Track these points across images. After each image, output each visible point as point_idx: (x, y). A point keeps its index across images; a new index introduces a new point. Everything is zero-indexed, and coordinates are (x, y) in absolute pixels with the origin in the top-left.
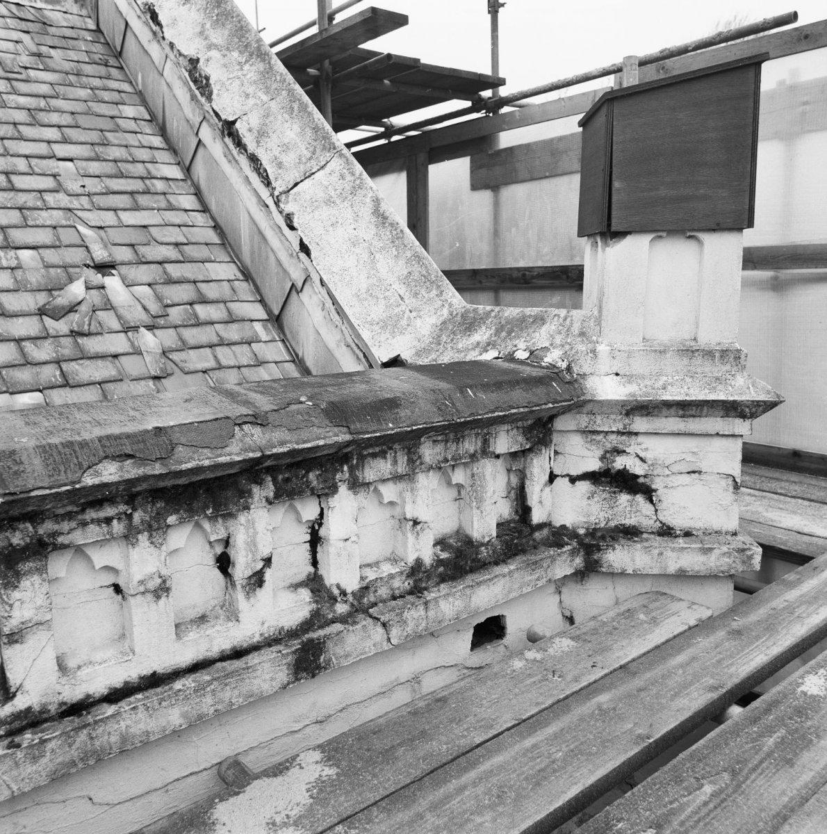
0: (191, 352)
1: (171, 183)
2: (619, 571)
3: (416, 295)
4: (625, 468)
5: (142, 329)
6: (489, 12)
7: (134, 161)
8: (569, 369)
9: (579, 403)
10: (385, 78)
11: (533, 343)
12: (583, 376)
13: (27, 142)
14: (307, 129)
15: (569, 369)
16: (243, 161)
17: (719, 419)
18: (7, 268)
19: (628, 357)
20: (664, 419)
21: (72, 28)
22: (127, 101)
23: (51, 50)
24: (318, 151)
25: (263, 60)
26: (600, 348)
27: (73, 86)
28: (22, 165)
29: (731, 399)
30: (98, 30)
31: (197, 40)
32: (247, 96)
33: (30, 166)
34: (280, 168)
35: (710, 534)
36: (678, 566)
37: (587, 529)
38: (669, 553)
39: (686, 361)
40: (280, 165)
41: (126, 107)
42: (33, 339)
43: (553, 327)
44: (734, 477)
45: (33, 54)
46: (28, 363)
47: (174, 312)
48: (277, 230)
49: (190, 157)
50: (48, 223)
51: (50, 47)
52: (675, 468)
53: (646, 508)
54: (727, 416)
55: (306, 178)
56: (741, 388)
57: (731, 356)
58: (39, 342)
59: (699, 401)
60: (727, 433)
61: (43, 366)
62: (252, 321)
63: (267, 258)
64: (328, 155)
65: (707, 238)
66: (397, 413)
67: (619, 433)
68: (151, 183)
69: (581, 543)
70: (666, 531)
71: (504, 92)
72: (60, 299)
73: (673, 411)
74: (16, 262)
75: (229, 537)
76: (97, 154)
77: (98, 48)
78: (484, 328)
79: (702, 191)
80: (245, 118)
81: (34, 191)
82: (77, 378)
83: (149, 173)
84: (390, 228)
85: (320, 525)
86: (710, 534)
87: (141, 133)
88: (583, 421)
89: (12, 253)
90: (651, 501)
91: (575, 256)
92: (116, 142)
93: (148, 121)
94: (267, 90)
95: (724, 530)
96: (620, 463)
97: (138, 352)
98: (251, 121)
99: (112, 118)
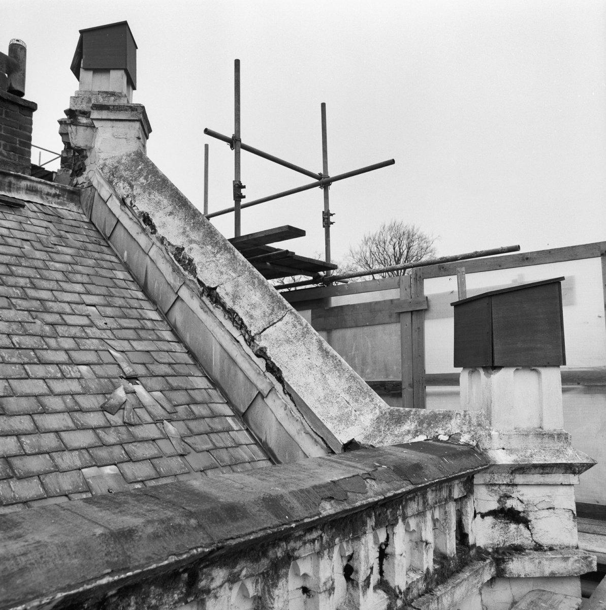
0: (197, 437)
1: (154, 322)
2: (517, 576)
3: (357, 401)
4: (512, 507)
5: (165, 421)
6: (324, 226)
7: (131, 308)
8: (477, 445)
9: (489, 466)
10: (268, 261)
11: (449, 431)
12: (485, 450)
13: (67, 293)
14: (266, 296)
15: (477, 445)
16: (219, 313)
17: (561, 475)
18: (75, 378)
19: (509, 438)
20: (531, 476)
21: (75, 220)
22: (117, 268)
23: (66, 233)
24: (275, 309)
25: (230, 252)
26: (493, 433)
27: (84, 257)
28: (67, 308)
29: (569, 462)
30: (91, 222)
31: (181, 237)
32: (222, 273)
33: (72, 309)
34: (252, 319)
35: (563, 548)
36: (550, 571)
37: (493, 548)
38: (544, 562)
39: (539, 440)
40: (251, 317)
41: (117, 272)
42: (103, 428)
43: (459, 421)
44: (572, 511)
45: (57, 236)
46: (104, 445)
47: (180, 409)
48: (248, 357)
49: (168, 308)
50: (92, 348)
51: (66, 232)
52: (540, 506)
53: (526, 533)
54: (566, 473)
55: (270, 326)
56: (570, 456)
57: (562, 437)
58: (106, 430)
59: (553, 464)
60: (566, 483)
61: (113, 447)
62: (226, 416)
63: (236, 375)
64: (283, 312)
65: (542, 370)
66: (424, 472)
67: (508, 485)
68: (144, 322)
69: (493, 558)
70: (538, 548)
71: (334, 273)
72: (112, 400)
73: (537, 470)
74: (79, 374)
75: (353, 554)
76: (108, 302)
77: (92, 233)
78: (409, 421)
79: (539, 345)
80: (222, 286)
81: (79, 326)
82: (135, 455)
83: (141, 315)
84: (331, 359)
85: (386, 545)
86: (563, 548)
87: (130, 289)
88: (487, 477)
89: (75, 368)
90: (528, 528)
91: (389, 375)
92: (118, 295)
93: (132, 281)
94: (235, 271)
95: (571, 545)
96: (509, 504)
97: (167, 437)
98: (226, 288)
99: (111, 278)
